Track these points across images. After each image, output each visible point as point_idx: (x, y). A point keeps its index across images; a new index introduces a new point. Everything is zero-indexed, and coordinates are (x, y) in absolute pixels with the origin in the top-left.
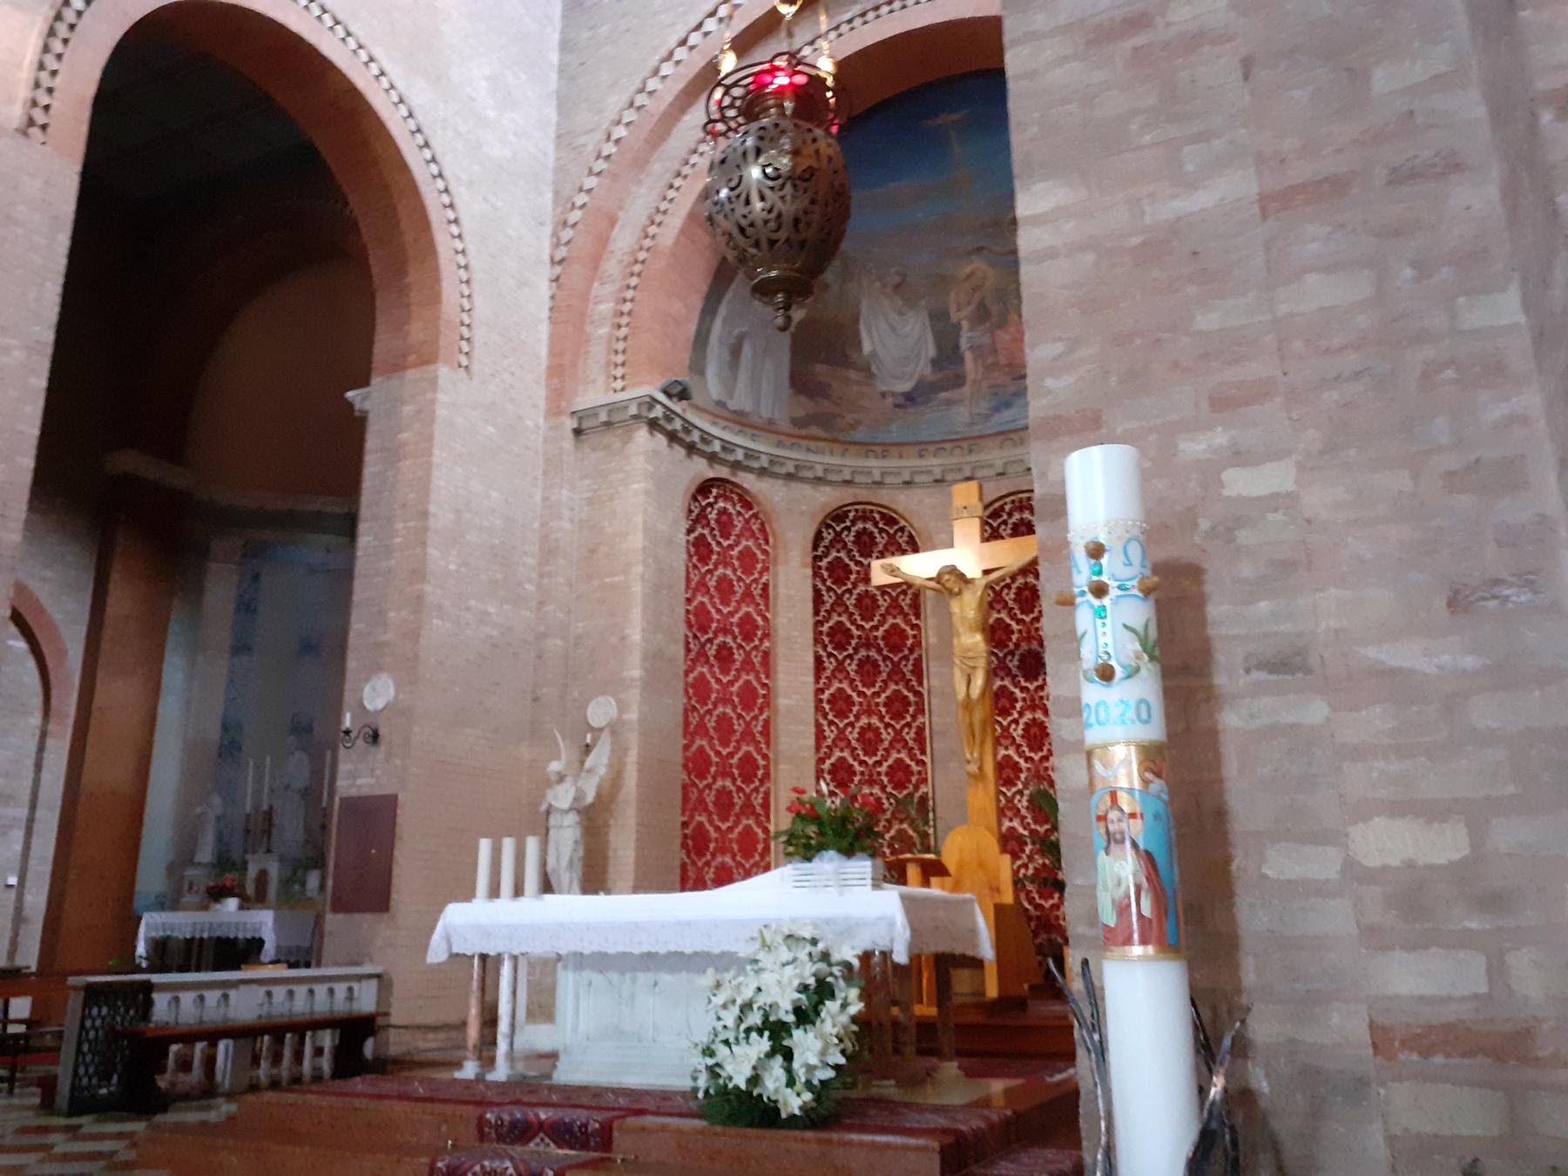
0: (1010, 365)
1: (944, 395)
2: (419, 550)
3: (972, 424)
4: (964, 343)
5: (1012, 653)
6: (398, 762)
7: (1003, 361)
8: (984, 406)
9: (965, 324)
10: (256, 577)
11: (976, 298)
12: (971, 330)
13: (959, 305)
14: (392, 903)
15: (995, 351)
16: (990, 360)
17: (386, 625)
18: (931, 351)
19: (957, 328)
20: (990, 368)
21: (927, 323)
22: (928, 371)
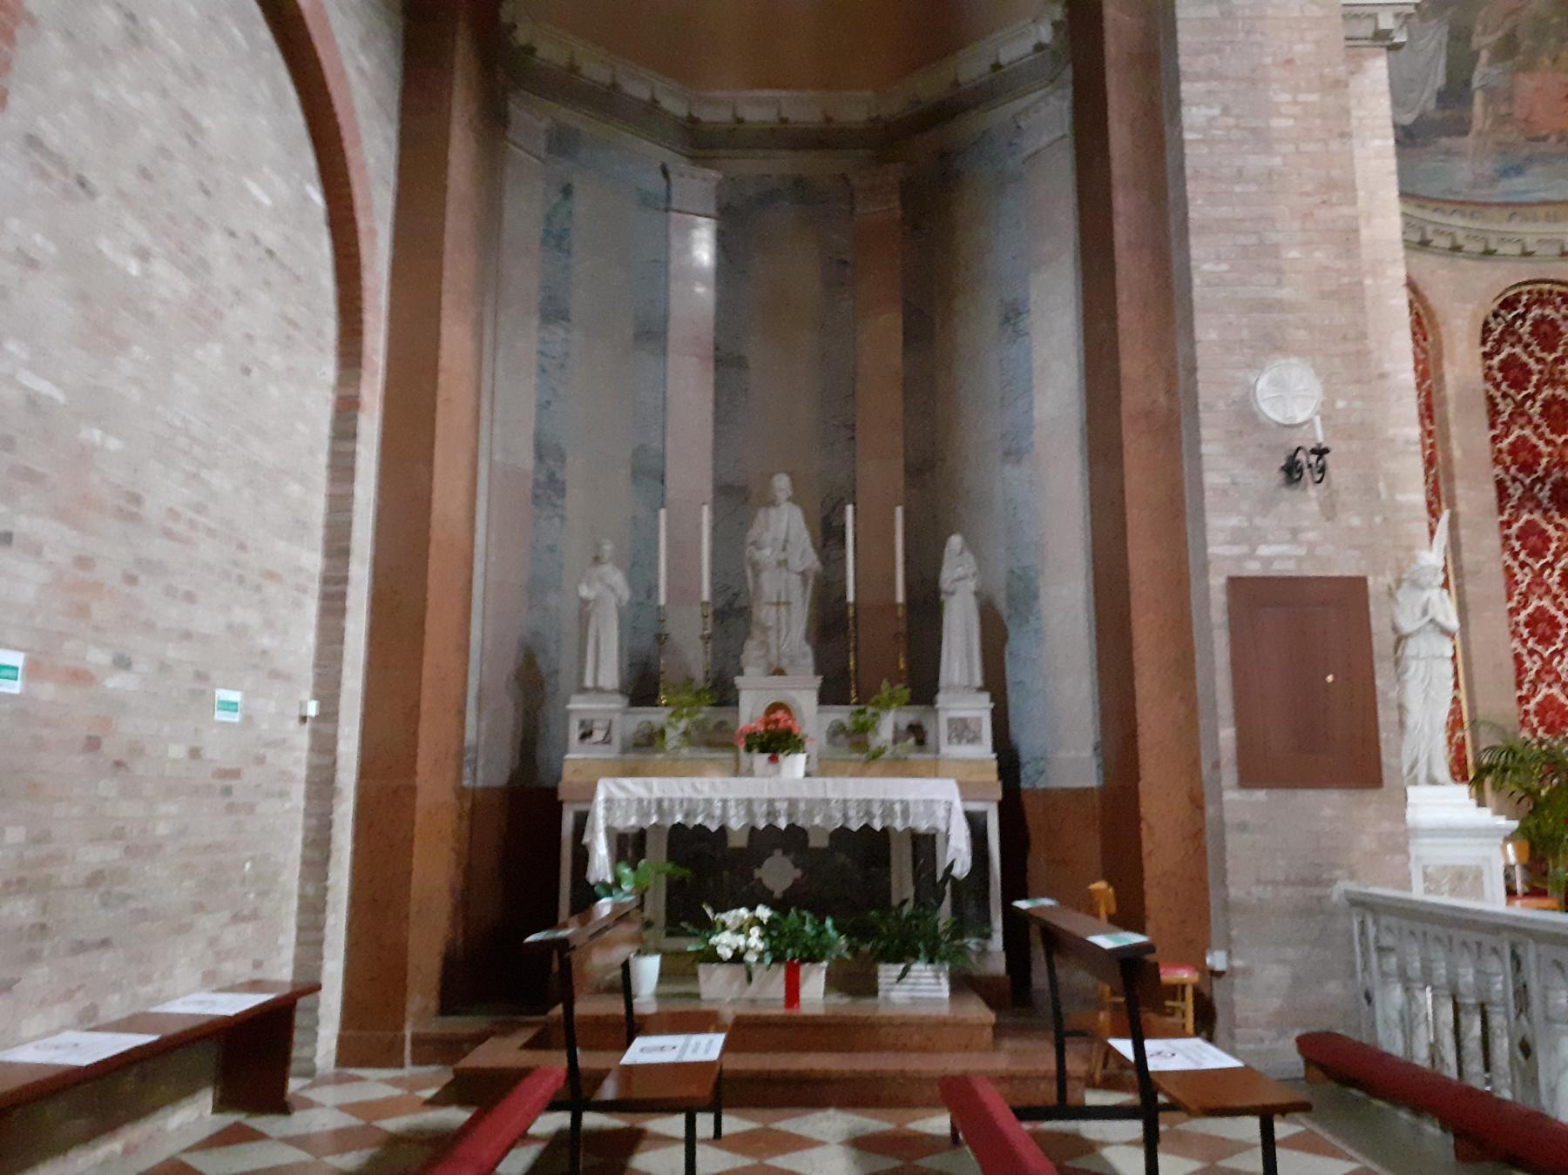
0: (1526, 120)
1: (1444, 141)
2: (1335, 146)
3: (1474, 185)
4: (1476, 82)
5: (1541, 480)
6: (1356, 521)
7: (1519, 113)
8: (1488, 167)
9: (1484, 55)
10: (567, 191)
11: (1508, 25)
12: (1490, 63)
13: (1486, 27)
14: (1386, 773)
15: (1510, 99)
16: (1503, 110)
17: (1279, 271)
18: (1439, 80)
19: (1475, 56)
20: (1503, 120)
21: (1445, 40)
22: (1431, 105)
